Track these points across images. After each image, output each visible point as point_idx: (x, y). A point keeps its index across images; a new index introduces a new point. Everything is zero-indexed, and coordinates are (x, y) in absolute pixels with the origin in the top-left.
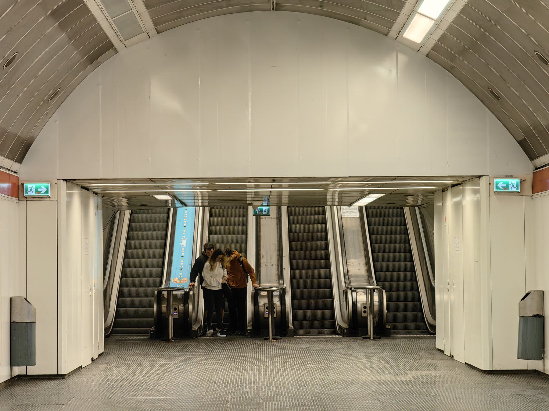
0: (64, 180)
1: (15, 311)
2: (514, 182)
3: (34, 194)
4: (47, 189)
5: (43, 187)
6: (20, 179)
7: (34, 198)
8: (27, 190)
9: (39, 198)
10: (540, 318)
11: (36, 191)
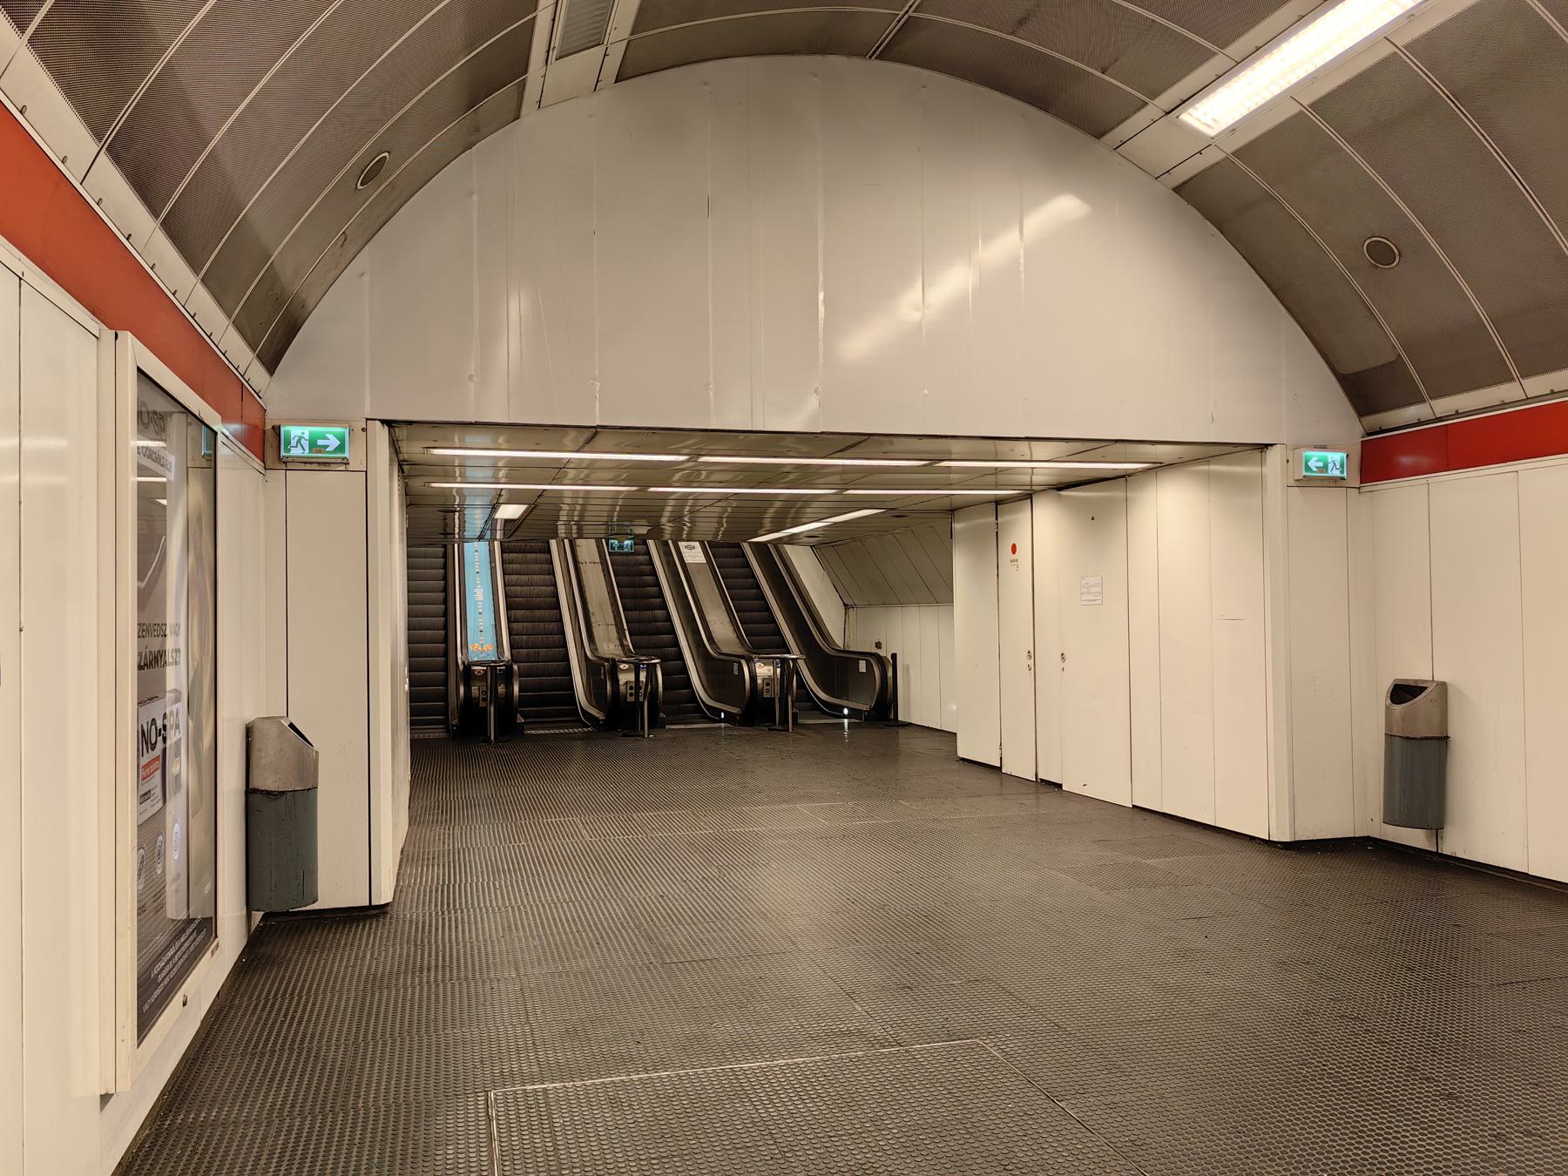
0: (383, 422)
1: (255, 772)
2: (1336, 457)
3: (307, 453)
4: (342, 441)
5: (330, 436)
6: (269, 414)
7: (306, 464)
8: (288, 442)
9: (319, 463)
10: (1444, 739)
11: (313, 445)
